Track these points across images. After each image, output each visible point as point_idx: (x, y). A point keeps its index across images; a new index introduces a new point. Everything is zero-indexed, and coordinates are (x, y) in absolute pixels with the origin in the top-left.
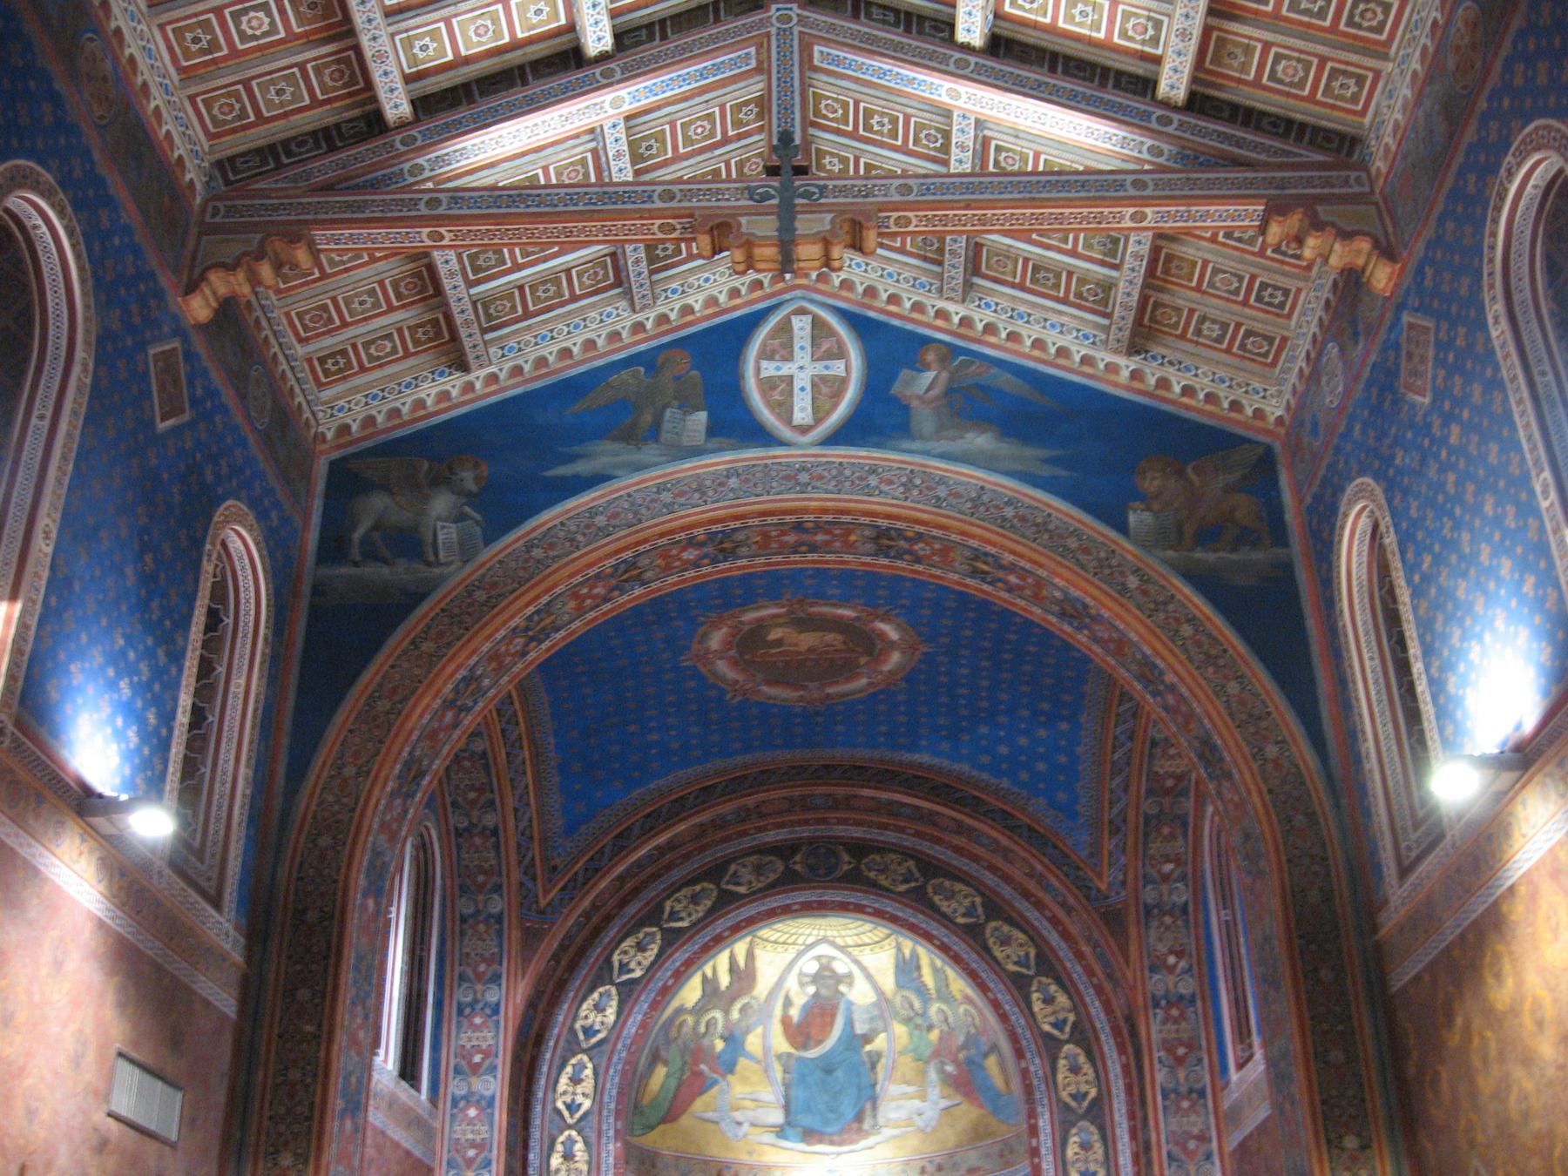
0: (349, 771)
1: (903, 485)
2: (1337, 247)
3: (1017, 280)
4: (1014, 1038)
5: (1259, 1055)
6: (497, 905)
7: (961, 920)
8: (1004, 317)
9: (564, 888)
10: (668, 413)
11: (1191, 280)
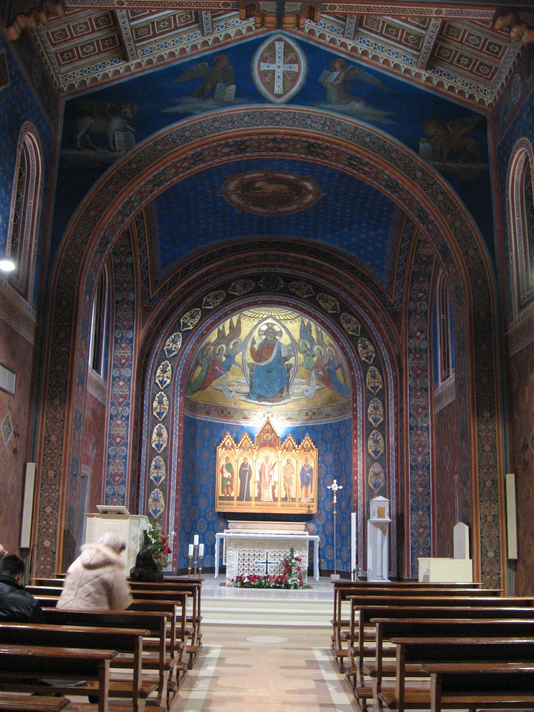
0: (78, 241)
1: (322, 124)
2: (526, 33)
3: (379, 31)
4: (349, 362)
5: (452, 376)
6: (132, 297)
7: (330, 312)
8: (371, 48)
9: (161, 290)
10: (218, 85)
11: (458, 38)
